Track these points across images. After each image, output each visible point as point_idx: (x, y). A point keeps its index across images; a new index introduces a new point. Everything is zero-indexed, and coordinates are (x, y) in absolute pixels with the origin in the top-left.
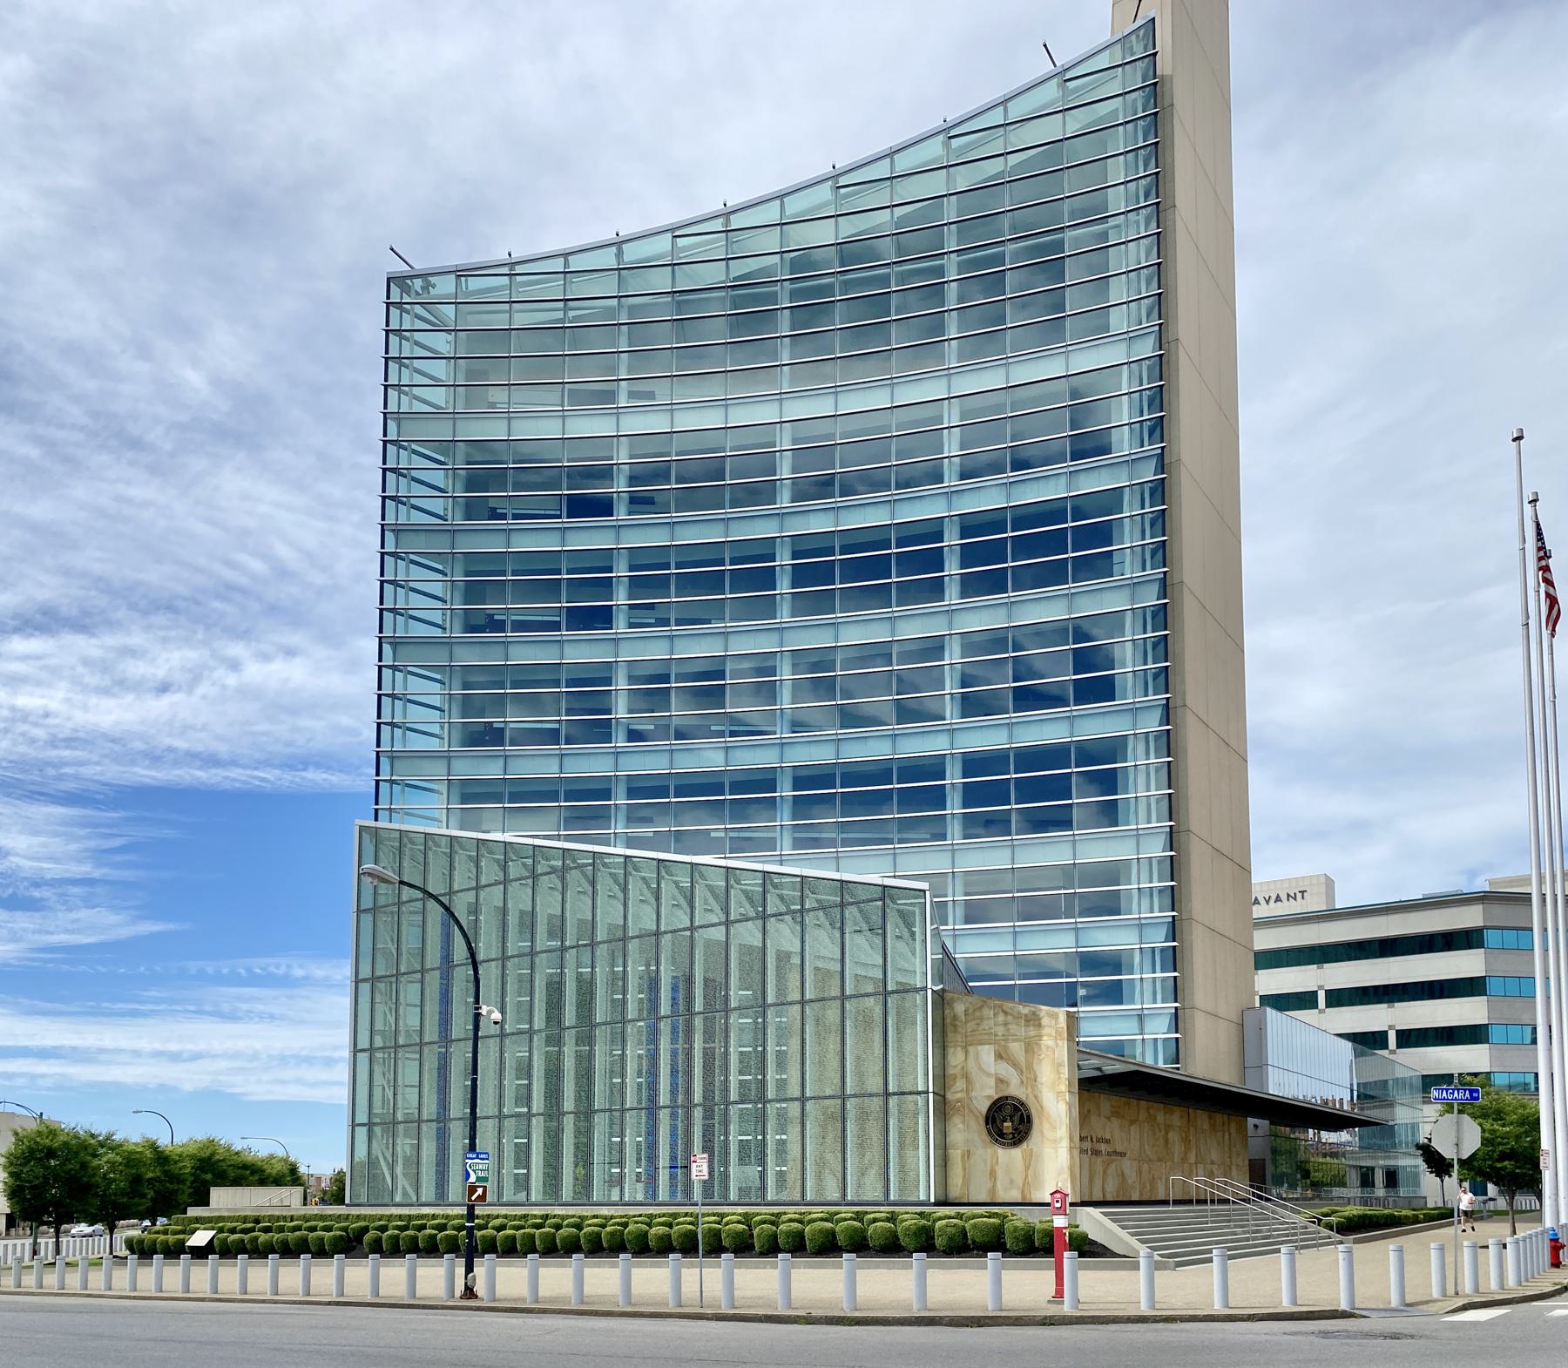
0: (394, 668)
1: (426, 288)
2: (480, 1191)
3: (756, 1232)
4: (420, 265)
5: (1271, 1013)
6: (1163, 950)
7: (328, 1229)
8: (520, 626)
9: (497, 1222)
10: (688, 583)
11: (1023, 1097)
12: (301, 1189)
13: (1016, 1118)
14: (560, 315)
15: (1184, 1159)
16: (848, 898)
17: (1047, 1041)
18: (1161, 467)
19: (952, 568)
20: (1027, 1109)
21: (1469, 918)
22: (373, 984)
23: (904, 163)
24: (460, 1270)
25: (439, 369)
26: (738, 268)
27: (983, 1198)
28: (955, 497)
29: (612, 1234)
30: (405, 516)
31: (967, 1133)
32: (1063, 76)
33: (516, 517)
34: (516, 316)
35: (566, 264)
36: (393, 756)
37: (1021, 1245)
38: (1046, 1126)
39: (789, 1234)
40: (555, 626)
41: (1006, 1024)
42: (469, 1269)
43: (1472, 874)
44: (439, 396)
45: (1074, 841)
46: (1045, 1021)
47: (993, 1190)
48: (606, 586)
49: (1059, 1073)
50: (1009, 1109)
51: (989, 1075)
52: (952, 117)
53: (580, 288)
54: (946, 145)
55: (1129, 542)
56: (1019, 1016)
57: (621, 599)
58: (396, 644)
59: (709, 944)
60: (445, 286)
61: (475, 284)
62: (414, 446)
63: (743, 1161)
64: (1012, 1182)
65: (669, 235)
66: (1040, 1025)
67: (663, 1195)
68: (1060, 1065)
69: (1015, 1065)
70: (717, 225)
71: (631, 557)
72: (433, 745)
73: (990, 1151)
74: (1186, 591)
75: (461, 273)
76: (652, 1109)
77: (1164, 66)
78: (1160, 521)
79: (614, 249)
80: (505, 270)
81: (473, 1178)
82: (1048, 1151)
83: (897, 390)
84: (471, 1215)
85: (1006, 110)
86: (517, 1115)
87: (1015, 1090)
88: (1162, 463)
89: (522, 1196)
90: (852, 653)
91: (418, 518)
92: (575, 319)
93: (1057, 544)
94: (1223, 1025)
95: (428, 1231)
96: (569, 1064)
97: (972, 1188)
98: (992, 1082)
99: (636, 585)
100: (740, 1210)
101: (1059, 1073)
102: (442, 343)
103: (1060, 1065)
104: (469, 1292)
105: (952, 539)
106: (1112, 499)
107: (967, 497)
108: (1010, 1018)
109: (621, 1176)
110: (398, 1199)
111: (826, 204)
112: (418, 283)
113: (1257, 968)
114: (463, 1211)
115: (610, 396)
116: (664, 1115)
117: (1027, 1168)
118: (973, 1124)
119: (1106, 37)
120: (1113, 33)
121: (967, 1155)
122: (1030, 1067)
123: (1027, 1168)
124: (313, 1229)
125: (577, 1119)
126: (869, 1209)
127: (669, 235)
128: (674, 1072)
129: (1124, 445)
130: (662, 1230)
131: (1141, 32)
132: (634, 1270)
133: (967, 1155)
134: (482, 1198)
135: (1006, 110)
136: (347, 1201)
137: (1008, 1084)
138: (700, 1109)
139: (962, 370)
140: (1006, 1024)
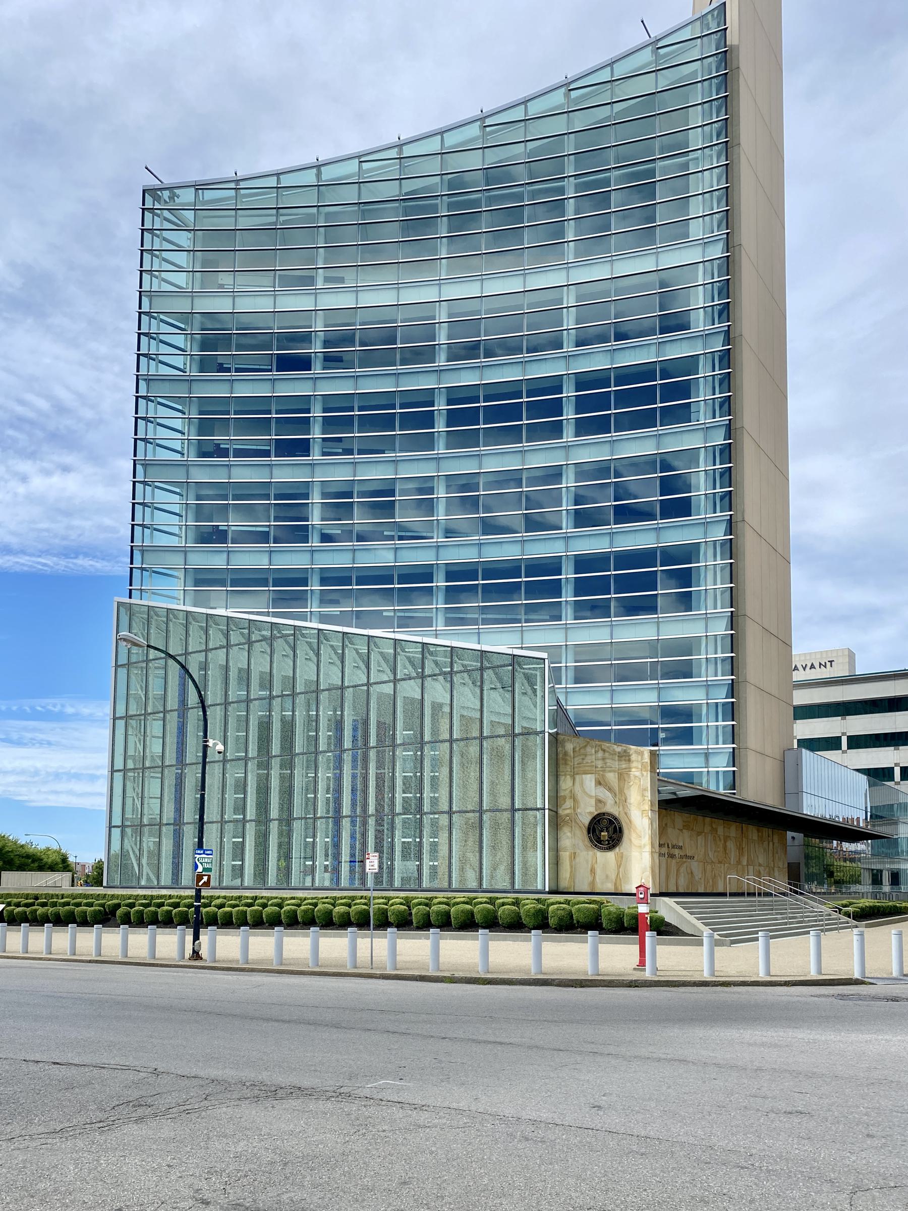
0: (144, 483)
1: (172, 198)
2: (205, 878)
4: (168, 181)
6: (724, 704)
7: (90, 905)
8: (239, 453)
9: (218, 902)
11: (616, 814)
14: (273, 219)
15: (739, 862)
17: (635, 772)
18: (728, 340)
23: (535, 108)
25: (182, 259)
26: (408, 186)
30: (154, 369)
31: (574, 839)
32: (655, 45)
34: (240, 220)
38: (633, 836)
39: (438, 913)
41: (604, 759)
42: (196, 937)
46: (634, 757)
47: (593, 883)
48: (305, 424)
51: (591, 797)
52: (571, 75)
55: (703, 396)
56: (614, 753)
57: (316, 434)
59: (380, 696)
60: (187, 196)
63: (405, 857)
64: (607, 876)
66: (629, 760)
69: (610, 789)
71: (324, 402)
73: (591, 853)
75: (199, 187)
76: (337, 819)
77: (732, 38)
78: (727, 381)
80: (233, 185)
81: (200, 869)
82: (635, 854)
84: (198, 897)
87: (610, 808)
89: (238, 882)
90: (491, 478)
91: (165, 371)
92: (285, 222)
93: (653, 396)
98: (593, 802)
99: (328, 424)
101: (643, 796)
104: (196, 955)
108: (607, 755)
109: (313, 868)
110: (143, 883)
112: (166, 194)
114: (192, 893)
115: (311, 281)
117: (619, 867)
119: (688, 16)
122: (621, 791)
123: (619, 867)
125: (280, 825)
129: (700, 323)
130: (343, 909)
131: (716, 13)
133: (574, 856)
134: (207, 884)
136: (105, 884)
137: (605, 804)
140: (604, 759)
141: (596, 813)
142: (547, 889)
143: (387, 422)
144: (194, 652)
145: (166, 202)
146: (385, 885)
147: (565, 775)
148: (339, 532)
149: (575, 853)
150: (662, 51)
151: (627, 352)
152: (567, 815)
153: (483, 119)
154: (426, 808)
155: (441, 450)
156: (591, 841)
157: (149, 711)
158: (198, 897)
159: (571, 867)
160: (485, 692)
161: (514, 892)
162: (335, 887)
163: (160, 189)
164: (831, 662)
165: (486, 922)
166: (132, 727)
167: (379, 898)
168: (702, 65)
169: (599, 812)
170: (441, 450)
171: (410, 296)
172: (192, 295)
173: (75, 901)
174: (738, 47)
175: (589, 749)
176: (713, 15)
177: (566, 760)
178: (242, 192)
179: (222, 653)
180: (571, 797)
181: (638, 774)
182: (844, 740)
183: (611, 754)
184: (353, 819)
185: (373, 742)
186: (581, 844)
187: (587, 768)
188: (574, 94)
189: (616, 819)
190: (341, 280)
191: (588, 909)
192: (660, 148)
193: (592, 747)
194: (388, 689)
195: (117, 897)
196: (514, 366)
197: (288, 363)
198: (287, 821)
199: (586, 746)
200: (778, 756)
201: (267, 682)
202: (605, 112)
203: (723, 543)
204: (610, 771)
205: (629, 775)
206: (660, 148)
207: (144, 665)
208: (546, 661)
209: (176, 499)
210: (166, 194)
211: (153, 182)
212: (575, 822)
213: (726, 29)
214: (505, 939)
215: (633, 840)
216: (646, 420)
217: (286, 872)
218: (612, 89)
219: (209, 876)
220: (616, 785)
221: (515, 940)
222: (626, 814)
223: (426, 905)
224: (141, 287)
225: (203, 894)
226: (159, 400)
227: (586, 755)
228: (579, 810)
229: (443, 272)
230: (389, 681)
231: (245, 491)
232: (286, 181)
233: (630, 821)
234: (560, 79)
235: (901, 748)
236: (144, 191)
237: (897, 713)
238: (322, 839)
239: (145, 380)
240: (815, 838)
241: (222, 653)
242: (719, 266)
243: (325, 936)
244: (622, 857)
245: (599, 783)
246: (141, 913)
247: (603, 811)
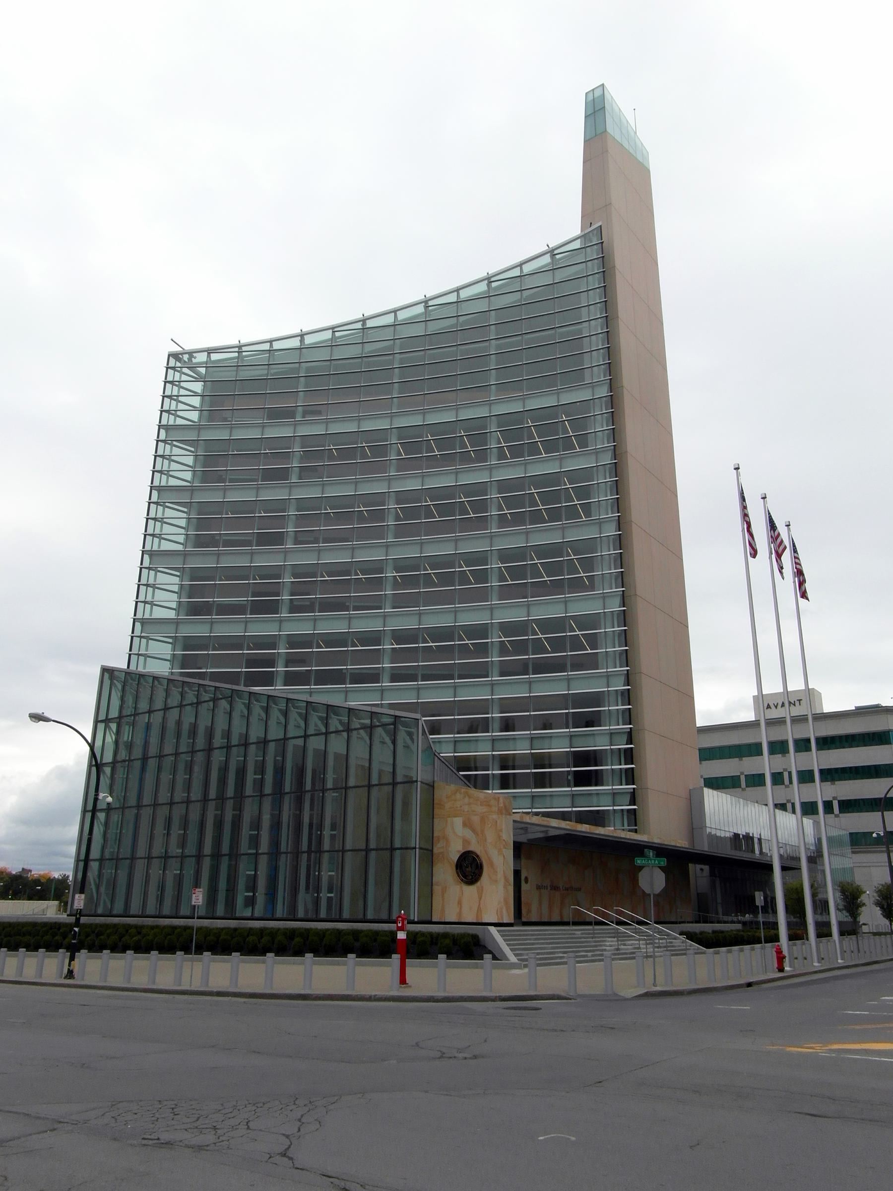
1: (190, 359)
4: (188, 347)
5: (707, 792)
8: (227, 543)
11: (479, 853)
12: (856, 870)
20: (480, 860)
26: (368, 348)
31: (445, 874)
35: (271, 346)
40: (248, 543)
42: (72, 958)
47: (460, 914)
48: (282, 520)
60: (202, 358)
62: (175, 443)
74: (634, 526)
75: (210, 351)
76: (199, 857)
85: (521, 269)
87: (474, 847)
96: (266, 819)
104: (70, 974)
110: (100, 911)
117: (480, 899)
122: (483, 831)
125: (230, 860)
133: (444, 890)
135: (521, 269)
139: (499, 401)
140: (469, 804)
163: (182, 354)
164: (800, 700)
171: (368, 426)
175: (458, 796)
182: (743, 778)
194: (300, 742)
197: (272, 475)
198: (216, 856)
201: (593, 641)
210: (186, 357)
211: (177, 349)
217: (230, 903)
236: (169, 356)
241: (176, 711)
242: (606, 402)
243: (115, 958)
245: (465, 825)
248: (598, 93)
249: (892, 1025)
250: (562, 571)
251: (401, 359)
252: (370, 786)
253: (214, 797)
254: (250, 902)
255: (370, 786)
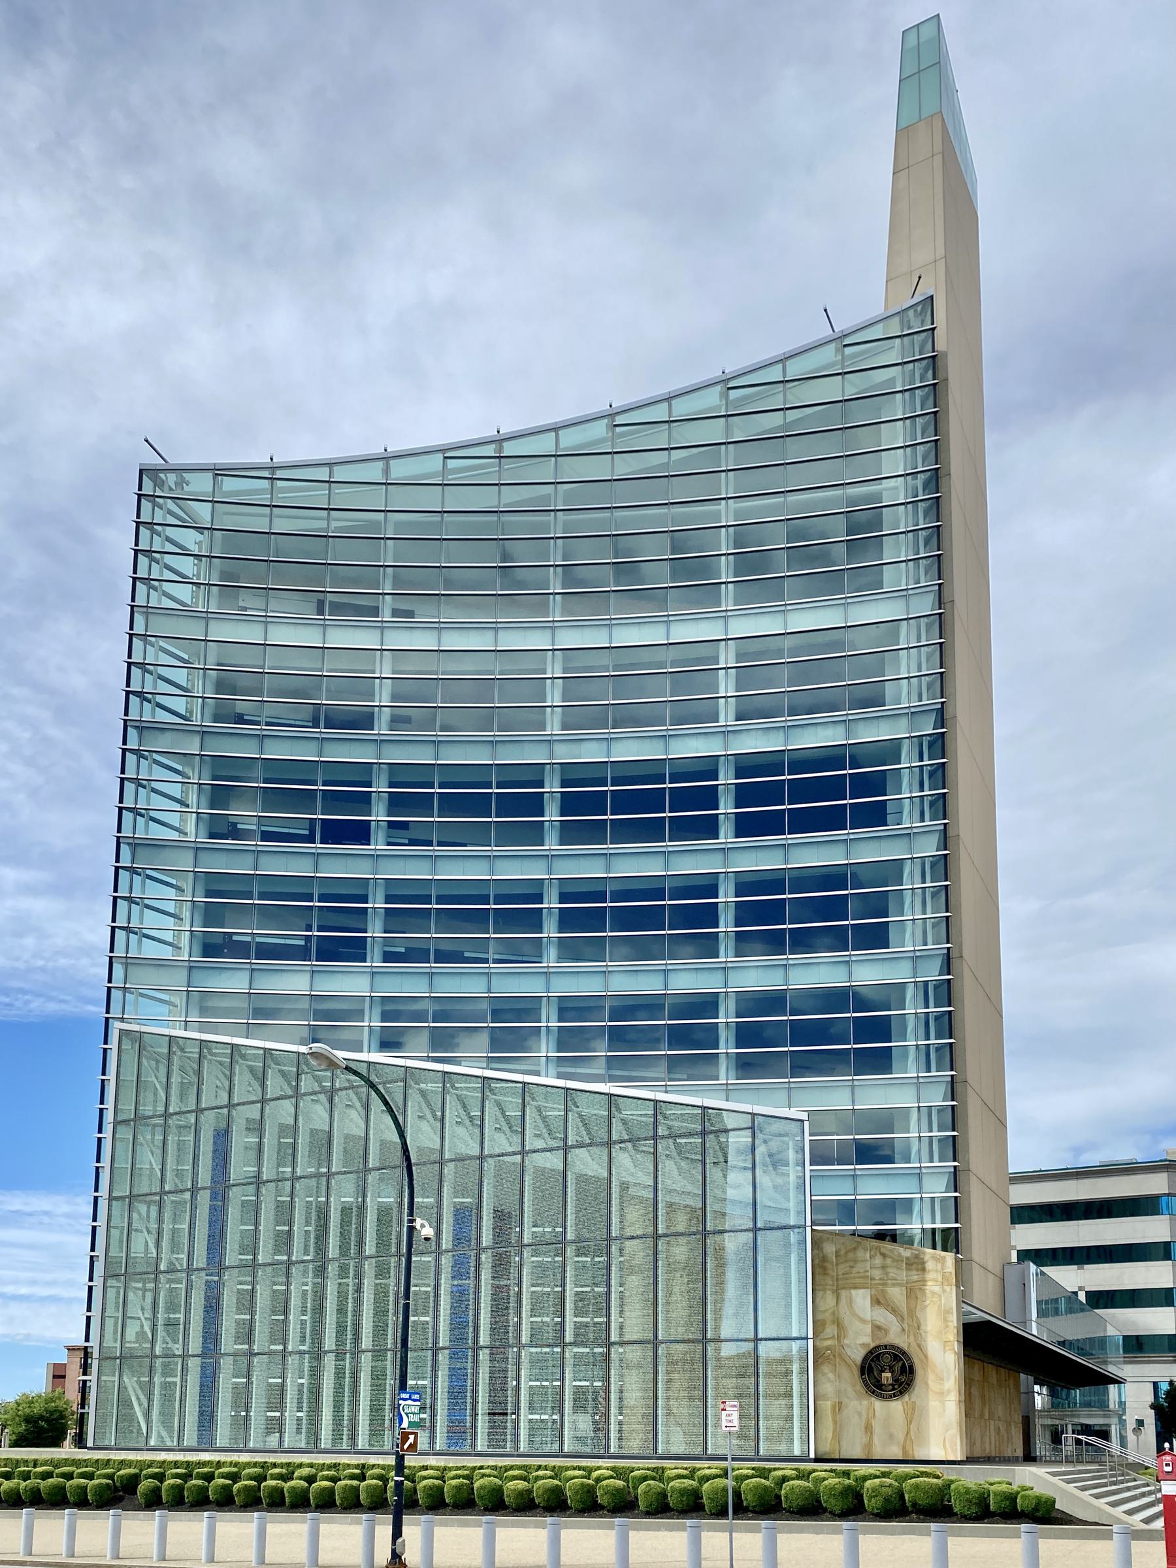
0: (132, 871)
2: (412, 1437)
3: (476, 1485)
4: (174, 460)
6: (943, 1200)
7: (90, 1476)
9: (305, 1471)
10: (451, 804)
11: (904, 1346)
13: (897, 1368)
14: (324, 524)
15: (982, 1415)
16: (708, 1127)
17: (932, 1287)
18: (941, 721)
19: (726, 808)
20: (909, 1359)
21: (1156, 1184)
22: (118, 1199)
23: (682, 408)
24: (384, 1531)
25: (187, 566)
27: (857, 1453)
28: (731, 736)
29: (459, 1488)
30: (148, 714)
31: (844, 1382)
32: (841, 341)
33: (268, 724)
34: (276, 520)
36: (127, 962)
37: (974, 1509)
38: (931, 1378)
39: (683, 1492)
41: (884, 1267)
42: (397, 1533)
43: (1077, 1151)
44: (184, 593)
45: (853, 1087)
46: (930, 1265)
47: (869, 1445)
49: (945, 1320)
50: (887, 1359)
51: (864, 1321)
52: (730, 369)
53: (343, 497)
54: (724, 395)
55: (906, 793)
56: (898, 1260)
57: (379, 815)
58: (135, 845)
59: (541, 1172)
60: (201, 484)
61: (229, 484)
63: (579, 1406)
64: (891, 1436)
65: (440, 456)
66: (924, 1270)
67: (325, 1441)
68: (948, 1312)
69: (894, 1311)
70: (489, 450)
71: (391, 774)
72: (166, 953)
73: (865, 1403)
75: (219, 472)
76: (317, 1355)
77: (941, 344)
78: (940, 775)
79: (380, 464)
80: (266, 474)
81: (405, 1424)
82: (933, 1404)
83: (673, 627)
84: (400, 1467)
85: (670, 406)
86: (270, 1353)
87: (895, 1337)
88: (941, 721)
89: (273, 1441)
90: (618, 886)
91: (163, 716)
92: (337, 529)
93: (838, 790)
94: (991, 1277)
95: (76, 1481)
97: (844, 1444)
98: (868, 1329)
99: (396, 803)
100: (491, 1462)
101: (945, 1320)
102: (190, 539)
103: (948, 1312)
105: (726, 779)
106: (891, 751)
107: (743, 737)
108: (889, 1261)
109: (281, 1420)
110: (152, 1443)
111: (602, 441)
112: (171, 478)
113: (1013, 1222)
114: (391, 1460)
115: (375, 611)
116: (329, 1362)
117: (909, 1423)
118: (845, 1373)
119: (878, 310)
120: (886, 308)
121: (839, 1407)
122: (911, 1313)
123: (909, 1423)
124: (69, 1476)
126: (777, 1465)
127: (440, 456)
128: (341, 1311)
129: (903, 696)
130: (521, 1485)
131: (919, 308)
132: (632, 1534)
133: (839, 1407)
134: (413, 1447)
136: (90, 1444)
137: (886, 1331)
138: (332, 1356)
140: (884, 1267)
141: (873, 1345)
142: (812, 1456)
143: (480, 805)
144: (243, 1104)
145: (171, 489)
146: (509, 1448)
147: (825, 1290)
148: (403, 950)
149: (840, 1403)
150: (848, 350)
151: (811, 730)
152: (828, 1348)
153: (612, 416)
154: (569, 1338)
155: (552, 845)
156: (866, 1385)
157: (167, 1189)
158: (400, 1467)
159: (835, 1422)
160: (708, 1166)
161: (519, 1456)
162: (312, 1447)
165: (762, 1505)
166: (140, 1214)
167: (574, 1469)
168: (903, 373)
169: (877, 1343)
170: (552, 845)
172: (206, 617)
173: (39, 1470)
174: (945, 354)
176: (916, 311)
177: (825, 1268)
178: (280, 483)
179: (288, 1105)
180: (833, 1322)
181: (937, 1289)
183: (894, 1260)
184: (339, 1355)
185: (370, 1249)
186: (850, 1389)
187: (858, 1280)
188: (733, 394)
189: (904, 1353)
190: (410, 614)
191: (931, 1486)
192: (872, 464)
193: (865, 1249)
195: (130, 1464)
196: (655, 741)
199: (855, 1249)
200: (998, 1271)
202: (776, 419)
203: (938, 985)
204: (894, 1285)
205: (923, 1291)
206: (872, 464)
207: (161, 1121)
208: (806, 1124)
209: (171, 893)
212: (840, 1355)
213: (933, 329)
214: (801, 1531)
215: (930, 1383)
216: (831, 820)
218: (785, 391)
219: (416, 1434)
220: (904, 1305)
221: (817, 1532)
222: (919, 1346)
223: (525, 1479)
224: (133, 600)
225: (406, 1463)
226: (155, 756)
227: (856, 1261)
228: (846, 1341)
229: (558, 612)
230: (558, 1149)
231: (275, 887)
232: (340, 474)
233: (926, 1357)
234: (716, 374)
235: (1086, 1266)
236: (141, 471)
237: (1081, 1222)
238: (296, 1381)
239: (136, 727)
240: (1041, 1385)
241: (288, 1105)
244: (914, 1409)
245: (876, 1302)
246: (227, 1489)
247: (884, 1342)
248: (928, 32)
249: (7, 1485)
250: (843, 912)
251: (565, 524)
252: (656, 1237)
253: (490, 1244)
254: (276, 1426)
255: (656, 1237)
